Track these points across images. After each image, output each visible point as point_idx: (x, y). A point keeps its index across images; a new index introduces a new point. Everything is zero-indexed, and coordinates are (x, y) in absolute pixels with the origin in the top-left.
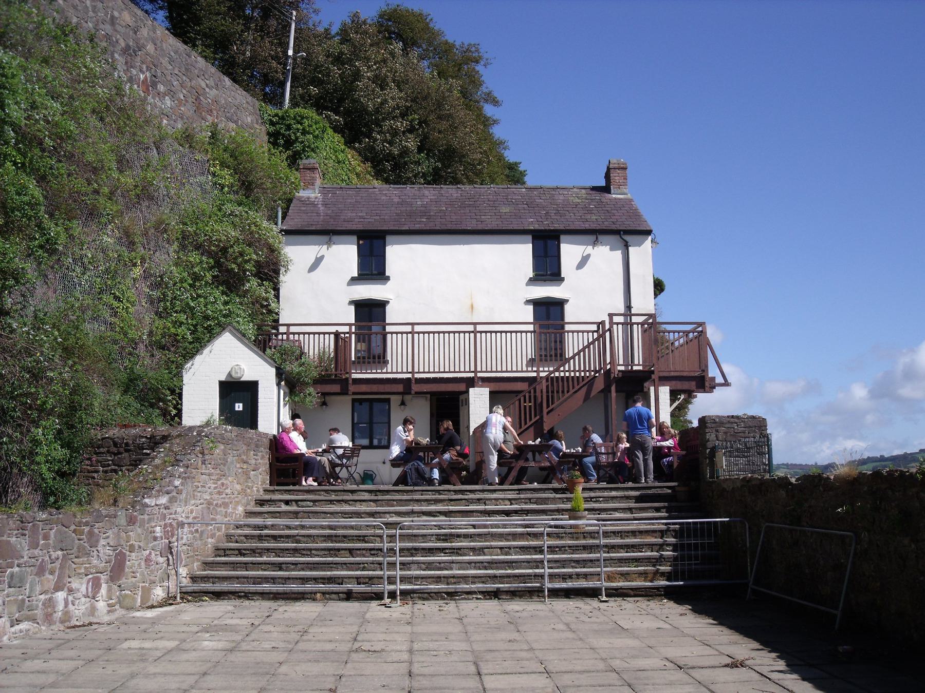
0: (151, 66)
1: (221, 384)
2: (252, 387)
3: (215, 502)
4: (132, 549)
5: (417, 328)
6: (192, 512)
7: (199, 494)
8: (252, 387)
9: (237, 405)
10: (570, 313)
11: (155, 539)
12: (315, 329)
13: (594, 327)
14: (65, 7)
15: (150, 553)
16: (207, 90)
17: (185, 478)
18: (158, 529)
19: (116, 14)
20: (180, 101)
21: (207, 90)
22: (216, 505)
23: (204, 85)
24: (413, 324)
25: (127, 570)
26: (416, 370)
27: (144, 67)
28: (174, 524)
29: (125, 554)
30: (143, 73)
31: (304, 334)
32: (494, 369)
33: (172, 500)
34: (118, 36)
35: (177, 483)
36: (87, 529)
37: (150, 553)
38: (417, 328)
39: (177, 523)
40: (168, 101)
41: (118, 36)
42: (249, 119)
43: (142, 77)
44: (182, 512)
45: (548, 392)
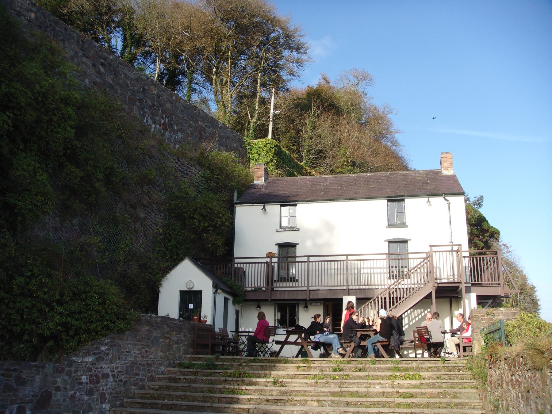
0: (169, 115)
1: (183, 293)
2: (199, 294)
3: (138, 363)
4: (58, 389)
5: (311, 259)
6: (117, 368)
7: (124, 357)
8: (199, 294)
9: (190, 305)
10: (411, 247)
11: (81, 383)
12: (253, 261)
13: (424, 256)
14: (113, 84)
15: (75, 393)
16: (207, 128)
17: (111, 346)
18: (84, 378)
19: (146, 88)
20: (187, 134)
21: (207, 128)
22: (140, 364)
23: (204, 126)
24: (308, 256)
25: (52, 403)
26: (310, 285)
27: (164, 115)
28: (101, 376)
29: (51, 393)
30: (163, 119)
31: (246, 263)
32: (342, 284)
33: (98, 359)
34: (147, 99)
35: (103, 348)
36: (14, 374)
37: (75, 393)
38: (311, 259)
39: (103, 375)
40: (180, 135)
41: (147, 99)
42: (235, 145)
43: (162, 121)
44: (106, 368)
45: (390, 298)
